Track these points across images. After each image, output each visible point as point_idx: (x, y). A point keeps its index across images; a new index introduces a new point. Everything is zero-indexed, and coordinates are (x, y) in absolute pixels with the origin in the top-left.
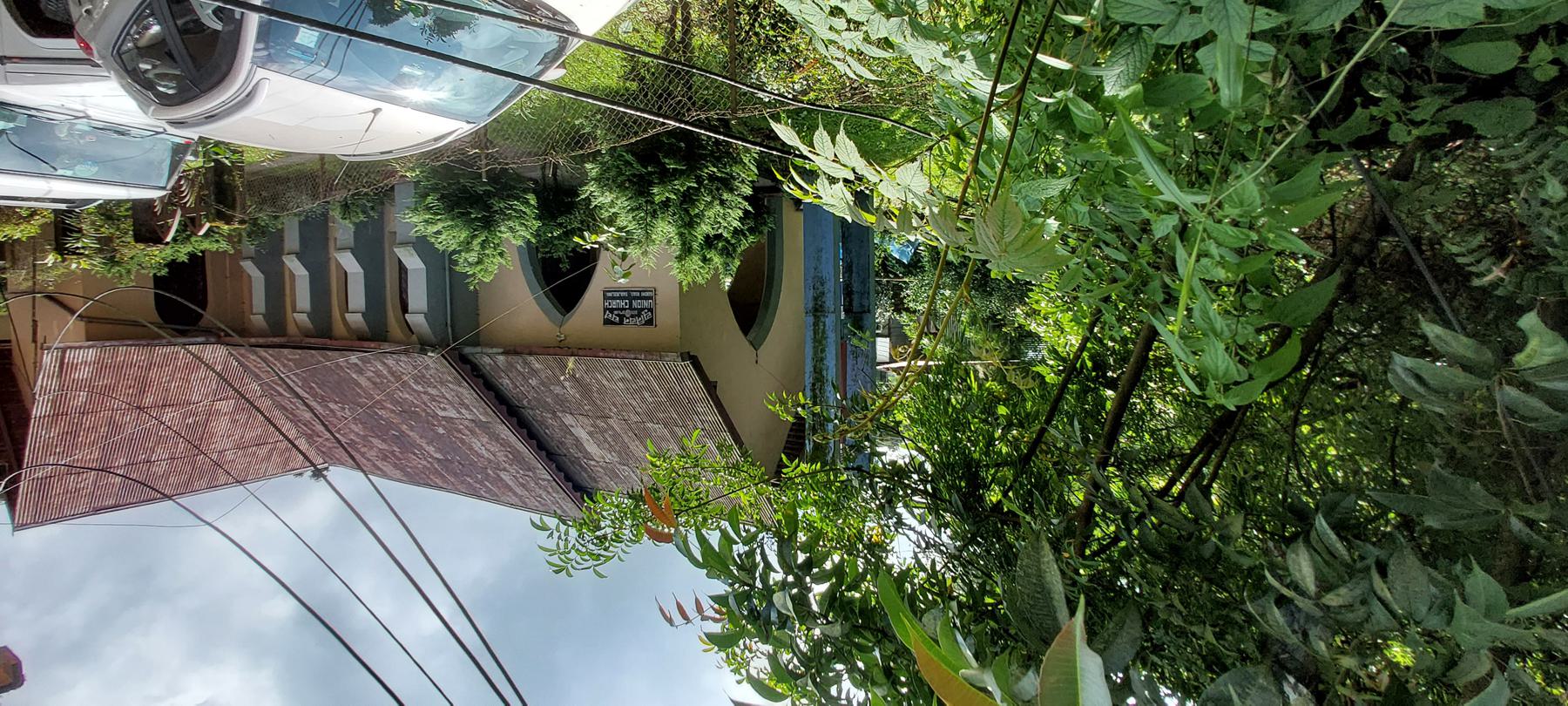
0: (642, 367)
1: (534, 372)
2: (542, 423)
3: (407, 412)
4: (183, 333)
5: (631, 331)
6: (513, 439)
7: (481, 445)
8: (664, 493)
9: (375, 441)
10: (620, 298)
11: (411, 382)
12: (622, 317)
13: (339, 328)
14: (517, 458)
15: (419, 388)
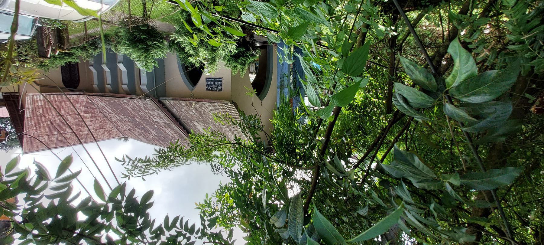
0: (217, 106)
1: (183, 107)
2: (188, 125)
4: (72, 91)
5: (215, 92)
6: (178, 130)
9: (136, 129)
10: (211, 81)
11: (144, 109)
12: (212, 88)
13: (121, 91)
14: (180, 136)
15: (146, 111)
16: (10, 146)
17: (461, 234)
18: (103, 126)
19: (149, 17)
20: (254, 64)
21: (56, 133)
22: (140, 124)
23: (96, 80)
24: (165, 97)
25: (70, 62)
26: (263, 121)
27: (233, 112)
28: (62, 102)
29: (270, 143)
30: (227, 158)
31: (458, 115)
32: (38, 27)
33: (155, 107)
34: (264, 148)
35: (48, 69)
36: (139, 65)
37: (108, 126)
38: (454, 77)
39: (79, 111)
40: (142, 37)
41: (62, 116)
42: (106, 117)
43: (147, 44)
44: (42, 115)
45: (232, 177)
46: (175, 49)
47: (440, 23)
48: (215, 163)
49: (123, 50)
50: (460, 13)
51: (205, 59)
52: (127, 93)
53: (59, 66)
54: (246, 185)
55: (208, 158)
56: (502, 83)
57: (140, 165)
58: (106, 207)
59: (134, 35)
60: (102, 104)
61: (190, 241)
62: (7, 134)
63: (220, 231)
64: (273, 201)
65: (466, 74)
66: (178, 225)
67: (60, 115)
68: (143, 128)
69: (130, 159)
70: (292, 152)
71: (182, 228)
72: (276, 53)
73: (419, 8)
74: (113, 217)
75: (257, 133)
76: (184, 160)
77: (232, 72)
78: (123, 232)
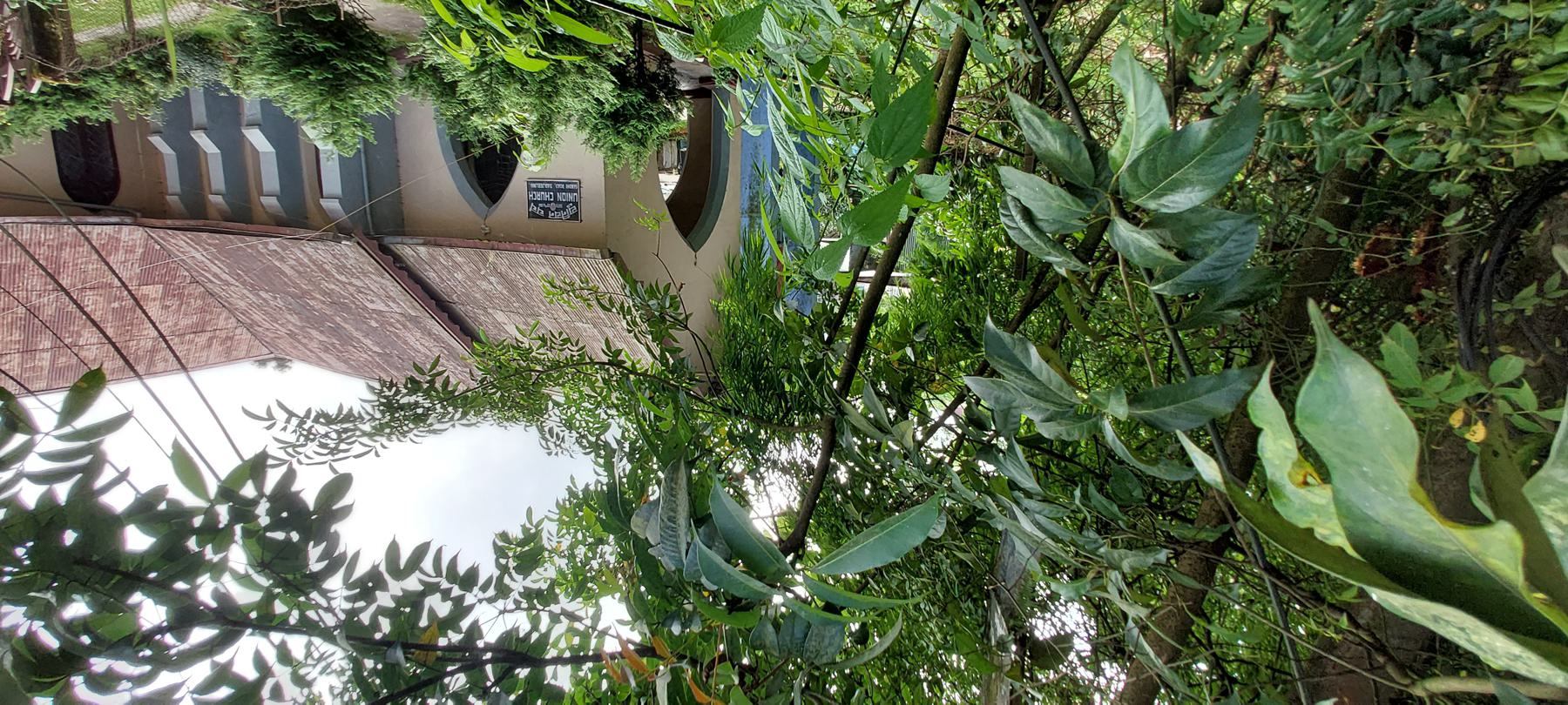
0: (564, 264)
1: (457, 266)
2: (476, 320)
3: (338, 304)
4: (95, 212)
5: (557, 224)
6: (444, 335)
8: (418, 377)
9: (314, 333)
10: (544, 190)
11: (334, 272)
12: (546, 210)
15: (343, 279)
21: (48, 344)
22: (324, 318)
23: (173, 180)
24: (404, 234)
25: (81, 120)
27: (612, 281)
28: (61, 247)
33: (369, 265)
36: (313, 133)
37: (221, 323)
38: (1126, 142)
39: (124, 275)
40: (320, 46)
43: (336, 68)
49: (256, 89)
53: (44, 129)
56: (1224, 156)
57: (322, 429)
58: (210, 514)
59: (292, 37)
60: (198, 256)
66: (427, 564)
68: (336, 331)
69: (291, 414)
71: (439, 573)
76: (458, 416)
78: (264, 582)
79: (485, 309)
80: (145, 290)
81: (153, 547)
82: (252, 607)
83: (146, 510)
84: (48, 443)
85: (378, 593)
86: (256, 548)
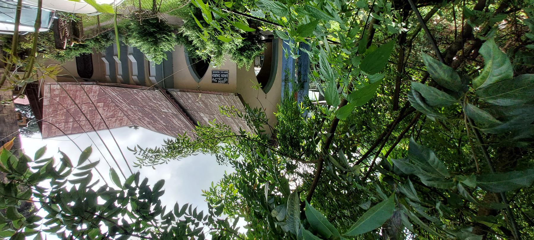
0: (223, 98)
4: (86, 81)
5: (221, 85)
6: (185, 120)
7: (175, 121)
9: (146, 118)
10: (217, 73)
12: (218, 80)
13: (132, 82)
14: (187, 126)
16: (30, 131)
17: (466, 233)
18: (115, 115)
19: (159, 11)
20: (259, 58)
21: (72, 120)
23: (108, 71)
25: (84, 53)
26: (268, 116)
28: (77, 91)
29: (274, 136)
30: (232, 149)
31: (480, 117)
32: (55, 20)
34: (268, 141)
35: (64, 60)
36: (149, 57)
37: (119, 115)
39: (93, 100)
40: (152, 30)
41: (77, 105)
42: (118, 106)
43: (156, 37)
44: (59, 103)
45: (237, 168)
46: (182, 41)
47: (453, 18)
48: (220, 154)
49: (134, 43)
50: (476, 8)
51: (211, 52)
52: (137, 84)
54: (251, 175)
55: (214, 150)
57: (150, 155)
58: (122, 193)
59: (143, 28)
61: (198, 227)
62: (27, 120)
63: (227, 219)
64: (276, 192)
65: (499, 77)
66: (187, 211)
67: (75, 104)
68: (152, 118)
69: (141, 150)
70: (296, 145)
72: (281, 46)
73: (432, 3)
74: (128, 202)
75: (261, 126)
77: (237, 66)
78: (137, 216)
79: (197, 112)
80: (99, 104)
81: (105, 204)
82: (133, 224)
83: (103, 192)
84: (75, 171)
85: (172, 222)
86: (136, 205)
